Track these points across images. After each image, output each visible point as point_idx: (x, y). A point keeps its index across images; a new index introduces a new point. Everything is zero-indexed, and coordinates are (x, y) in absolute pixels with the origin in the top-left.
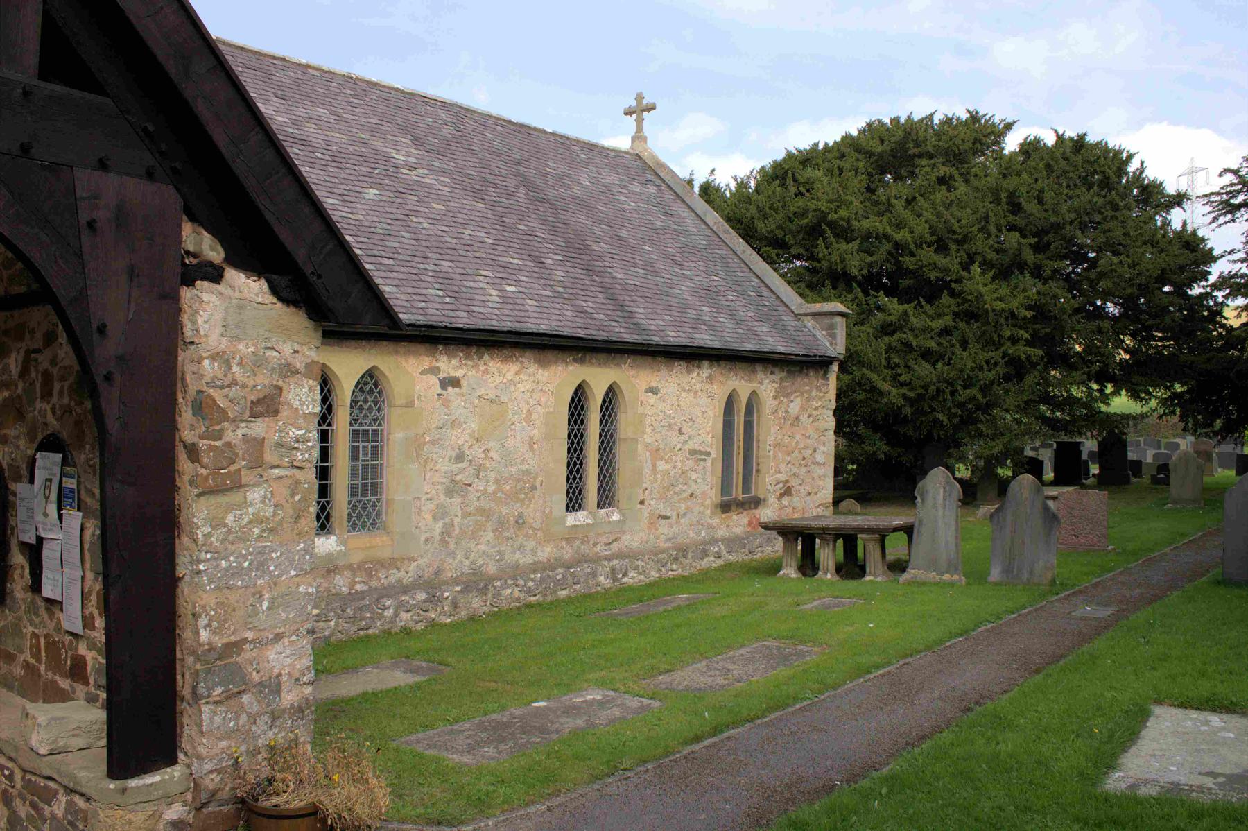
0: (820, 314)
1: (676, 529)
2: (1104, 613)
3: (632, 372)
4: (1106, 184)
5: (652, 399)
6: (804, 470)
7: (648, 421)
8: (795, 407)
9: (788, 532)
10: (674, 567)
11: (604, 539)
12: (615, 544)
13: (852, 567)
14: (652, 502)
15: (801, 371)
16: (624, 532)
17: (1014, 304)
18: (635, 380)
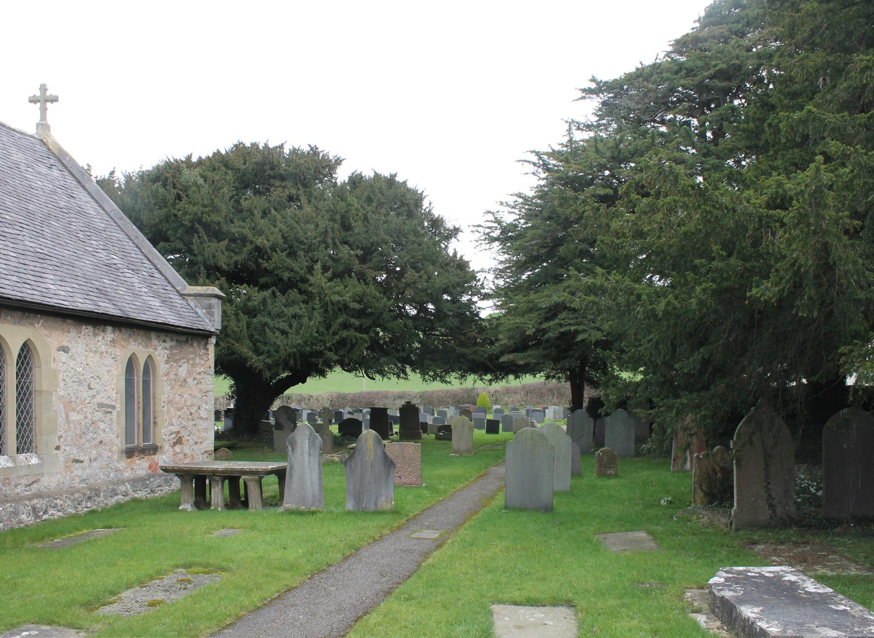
0: (201, 295)
1: (88, 471)
2: (434, 535)
3: (46, 332)
4: (410, 215)
5: (63, 356)
6: (191, 423)
7: (61, 377)
8: (183, 371)
9: (184, 474)
10: (89, 504)
11: (24, 481)
12: (35, 485)
13: (238, 501)
14: (68, 448)
15: (187, 341)
16: (43, 475)
17: (347, 297)
18: (48, 339)
